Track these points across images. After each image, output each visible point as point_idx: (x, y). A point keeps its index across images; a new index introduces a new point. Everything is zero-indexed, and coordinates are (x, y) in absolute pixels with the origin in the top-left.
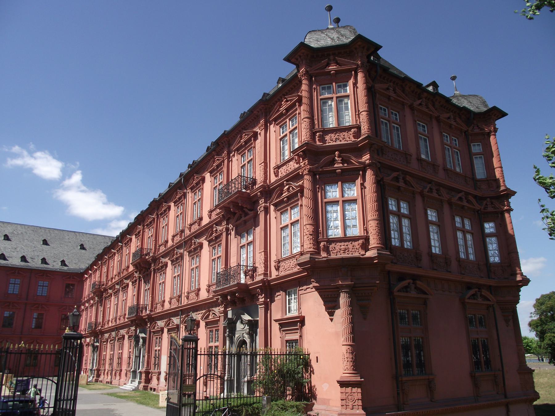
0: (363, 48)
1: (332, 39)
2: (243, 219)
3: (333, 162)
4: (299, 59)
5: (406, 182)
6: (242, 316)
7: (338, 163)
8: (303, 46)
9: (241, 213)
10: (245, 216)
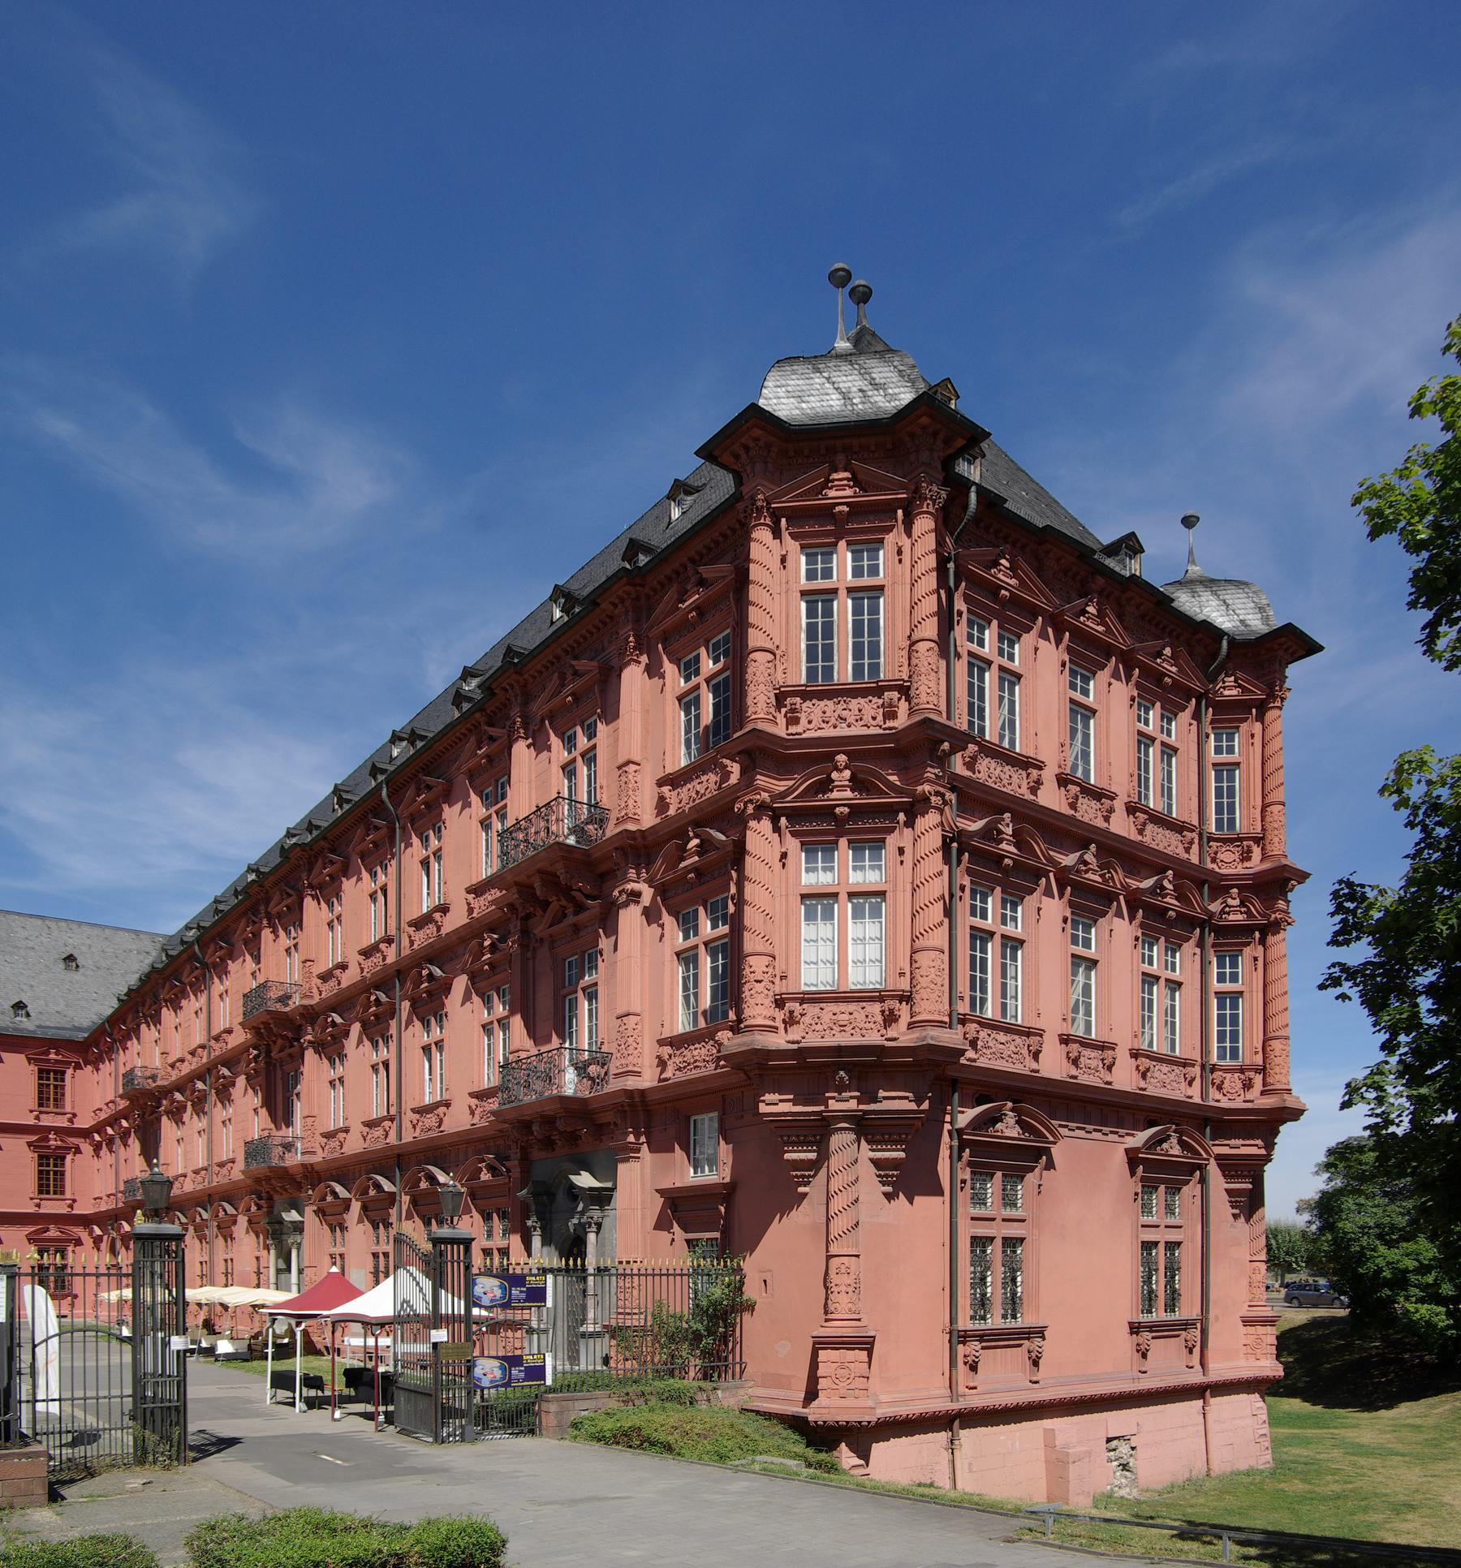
0: (935, 434)
1: (846, 396)
2: (571, 919)
3: (826, 785)
4: (744, 456)
6: (572, 1177)
7: (842, 788)
8: (755, 416)
9: (564, 902)
10: (576, 913)
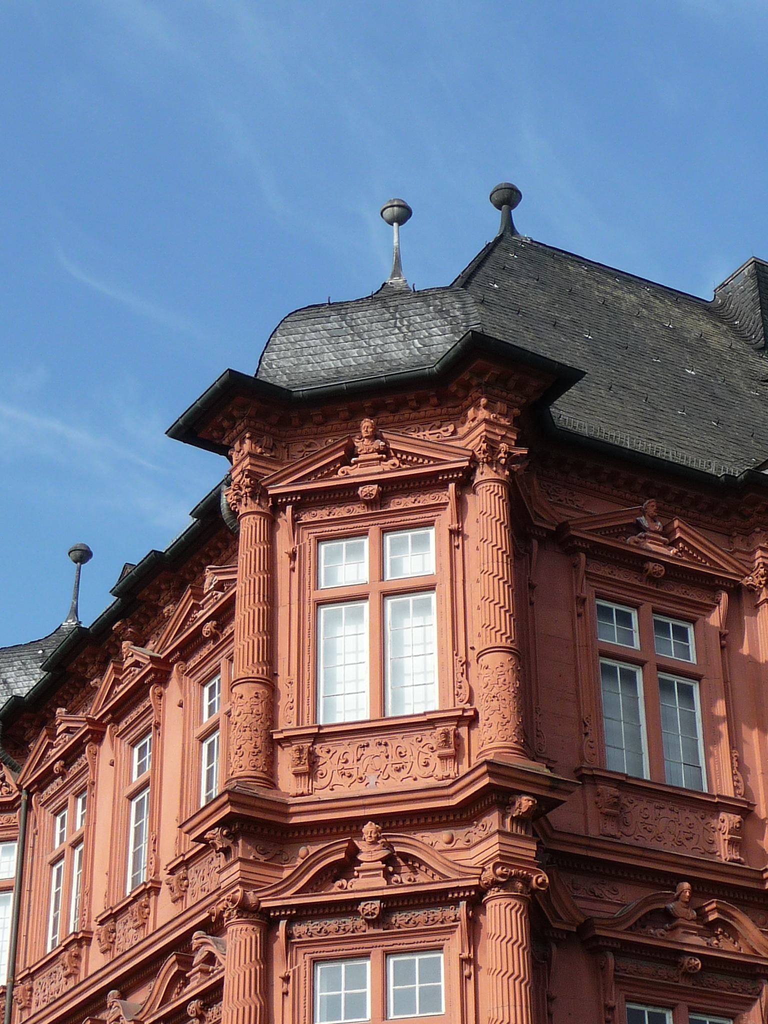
7: (367, 463)
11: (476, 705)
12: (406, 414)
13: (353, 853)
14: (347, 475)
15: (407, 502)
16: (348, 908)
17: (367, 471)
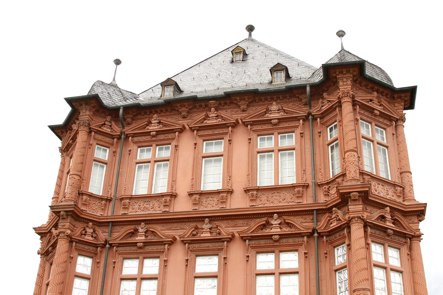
5: (395, 222)
11: (233, 188)
12: (168, 113)
13: (136, 230)
14: (148, 129)
15: (286, 125)
16: (270, 237)
17: (154, 127)
